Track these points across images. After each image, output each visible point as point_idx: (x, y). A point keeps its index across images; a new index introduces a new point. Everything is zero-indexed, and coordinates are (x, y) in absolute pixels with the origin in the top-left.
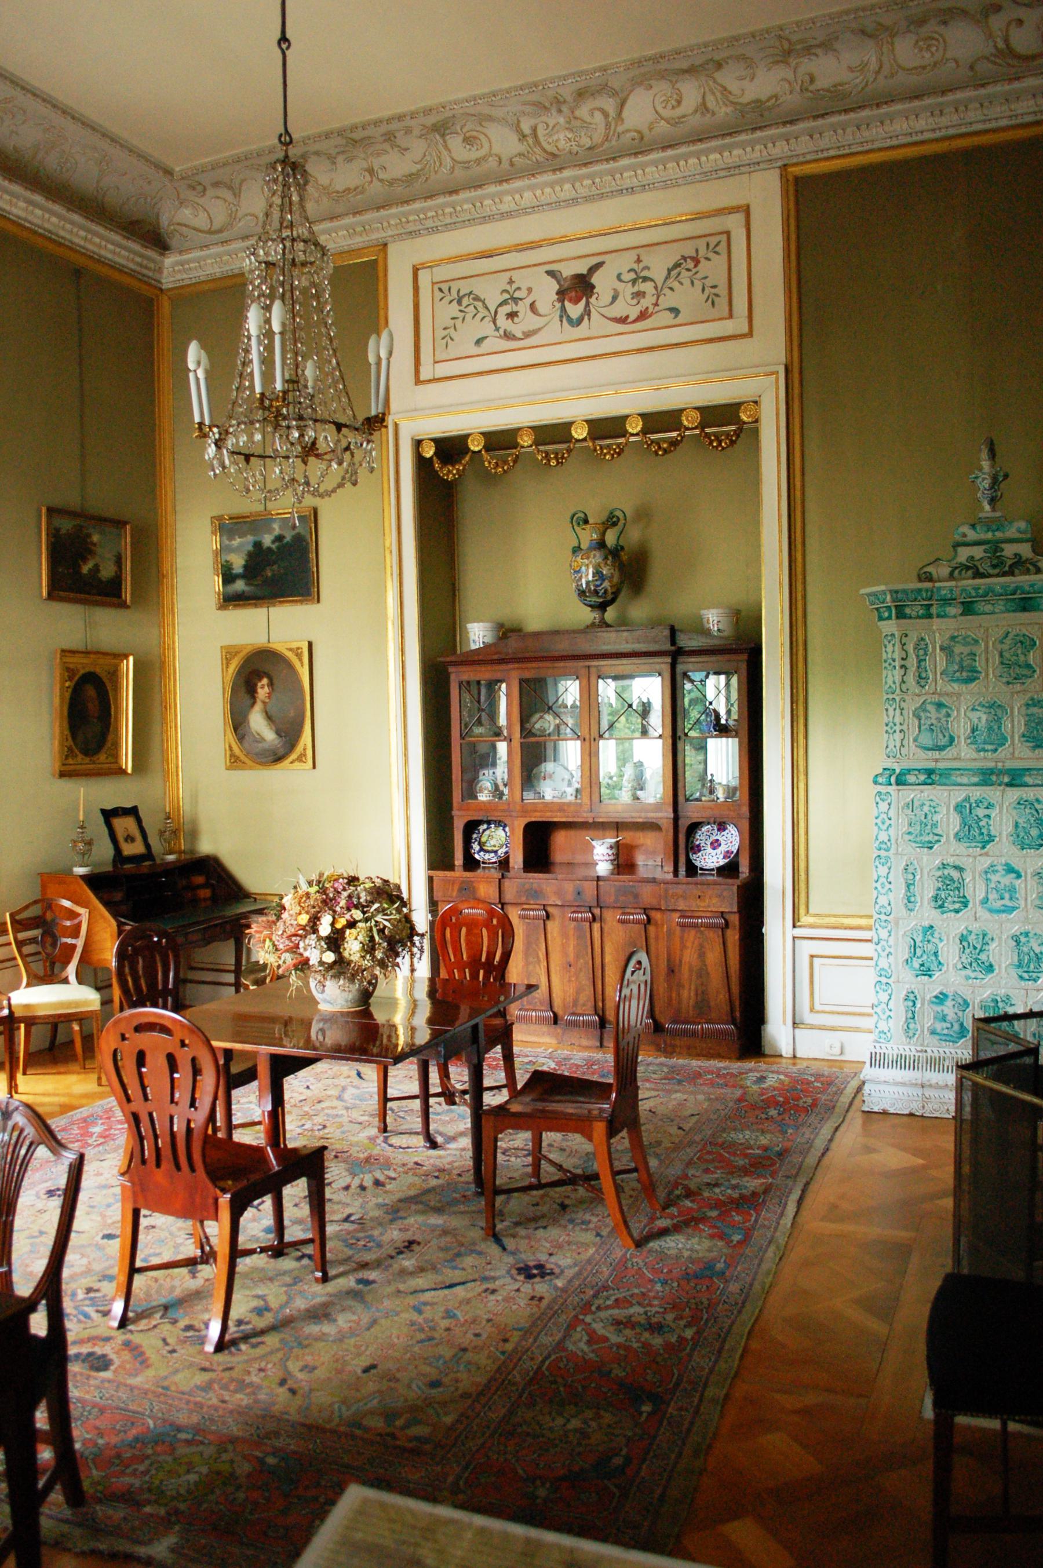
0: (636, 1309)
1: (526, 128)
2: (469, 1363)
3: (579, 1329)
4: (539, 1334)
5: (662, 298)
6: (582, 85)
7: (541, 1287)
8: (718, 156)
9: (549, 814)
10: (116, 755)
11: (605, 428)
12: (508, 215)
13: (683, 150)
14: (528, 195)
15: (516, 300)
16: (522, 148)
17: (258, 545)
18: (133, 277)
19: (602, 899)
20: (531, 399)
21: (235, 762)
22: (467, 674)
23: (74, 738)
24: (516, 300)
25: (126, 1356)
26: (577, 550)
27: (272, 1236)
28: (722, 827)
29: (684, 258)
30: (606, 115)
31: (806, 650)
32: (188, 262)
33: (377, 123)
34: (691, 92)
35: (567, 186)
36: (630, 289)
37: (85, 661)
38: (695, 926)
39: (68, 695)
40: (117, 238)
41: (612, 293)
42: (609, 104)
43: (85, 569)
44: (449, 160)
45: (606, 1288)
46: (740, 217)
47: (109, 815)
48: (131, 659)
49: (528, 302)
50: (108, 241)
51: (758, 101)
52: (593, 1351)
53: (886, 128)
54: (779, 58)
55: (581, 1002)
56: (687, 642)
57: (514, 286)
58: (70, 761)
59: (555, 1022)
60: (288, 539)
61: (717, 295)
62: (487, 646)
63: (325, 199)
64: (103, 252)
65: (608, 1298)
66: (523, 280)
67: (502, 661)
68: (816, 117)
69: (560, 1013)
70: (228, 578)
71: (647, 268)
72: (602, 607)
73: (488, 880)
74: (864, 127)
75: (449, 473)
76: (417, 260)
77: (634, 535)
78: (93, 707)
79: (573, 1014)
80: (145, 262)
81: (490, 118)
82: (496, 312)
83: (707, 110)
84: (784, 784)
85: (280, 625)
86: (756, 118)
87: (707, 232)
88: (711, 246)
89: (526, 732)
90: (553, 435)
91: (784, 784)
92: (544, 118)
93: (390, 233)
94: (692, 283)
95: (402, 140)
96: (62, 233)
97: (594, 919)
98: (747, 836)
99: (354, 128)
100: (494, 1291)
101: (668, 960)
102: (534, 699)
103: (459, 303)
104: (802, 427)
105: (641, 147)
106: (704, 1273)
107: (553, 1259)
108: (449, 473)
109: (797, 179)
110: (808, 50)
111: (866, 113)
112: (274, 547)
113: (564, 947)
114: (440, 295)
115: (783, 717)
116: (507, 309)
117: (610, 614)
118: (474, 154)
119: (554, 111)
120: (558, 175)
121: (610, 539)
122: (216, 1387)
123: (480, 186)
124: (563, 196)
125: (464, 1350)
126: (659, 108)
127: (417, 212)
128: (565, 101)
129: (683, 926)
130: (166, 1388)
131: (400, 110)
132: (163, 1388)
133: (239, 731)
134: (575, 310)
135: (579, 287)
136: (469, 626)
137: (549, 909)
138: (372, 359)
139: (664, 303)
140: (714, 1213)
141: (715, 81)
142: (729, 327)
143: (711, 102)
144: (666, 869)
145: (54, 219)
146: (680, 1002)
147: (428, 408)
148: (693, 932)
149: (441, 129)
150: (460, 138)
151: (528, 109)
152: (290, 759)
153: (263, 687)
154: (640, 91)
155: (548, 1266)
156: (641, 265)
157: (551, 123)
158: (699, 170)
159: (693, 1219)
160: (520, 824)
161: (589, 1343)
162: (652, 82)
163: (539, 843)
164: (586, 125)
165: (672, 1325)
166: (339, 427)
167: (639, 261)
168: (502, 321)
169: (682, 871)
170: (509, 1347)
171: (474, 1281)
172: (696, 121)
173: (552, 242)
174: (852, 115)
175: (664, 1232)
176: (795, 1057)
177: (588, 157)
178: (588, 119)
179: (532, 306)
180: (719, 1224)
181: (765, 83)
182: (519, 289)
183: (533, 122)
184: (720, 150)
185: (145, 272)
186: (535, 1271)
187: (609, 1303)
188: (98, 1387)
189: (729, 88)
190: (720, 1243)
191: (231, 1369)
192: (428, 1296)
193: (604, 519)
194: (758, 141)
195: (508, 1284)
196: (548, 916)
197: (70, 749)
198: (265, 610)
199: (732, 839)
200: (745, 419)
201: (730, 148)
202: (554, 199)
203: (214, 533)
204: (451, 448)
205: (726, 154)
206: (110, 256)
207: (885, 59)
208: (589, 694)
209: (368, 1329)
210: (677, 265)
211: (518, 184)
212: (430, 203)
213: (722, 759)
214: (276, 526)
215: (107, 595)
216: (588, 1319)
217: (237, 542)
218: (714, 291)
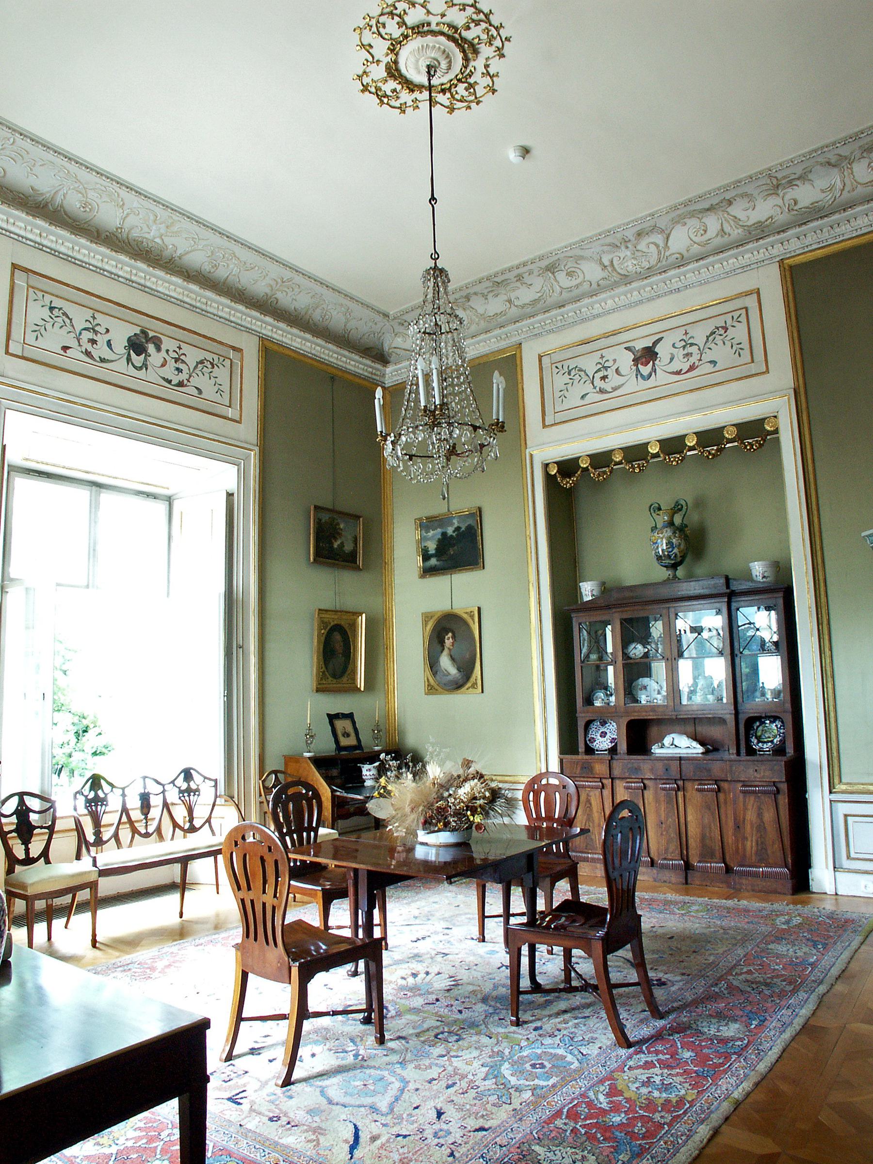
6: (638, 228)
10: (353, 679)
11: (673, 446)
12: (598, 316)
13: (711, 259)
15: (606, 368)
16: (605, 274)
17: (444, 534)
19: (683, 774)
20: (619, 429)
21: (431, 690)
24: (606, 368)
26: (654, 529)
29: (717, 328)
30: (657, 246)
31: (826, 586)
34: (713, 223)
36: (682, 352)
38: (754, 792)
39: (323, 639)
40: (357, 357)
41: (670, 356)
42: (659, 239)
43: (335, 546)
48: (364, 615)
51: (759, 222)
53: (852, 224)
54: (772, 192)
55: (671, 850)
56: (736, 586)
57: (604, 359)
59: (652, 865)
61: (741, 349)
63: (482, 322)
64: (349, 367)
66: (609, 354)
67: (608, 607)
68: (800, 225)
69: (656, 858)
70: (426, 557)
72: (674, 567)
73: (601, 761)
75: (567, 483)
76: (540, 351)
77: (694, 518)
78: (339, 647)
79: (665, 859)
81: (582, 258)
85: (458, 591)
86: (759, 232)
88: (735, 318)
90: (636, 453)
92: (616, 254)
93: (523, 336)
95: (527, 279)
97: (679, 789)
103: (569, 374)
104: (810, 429)
105: (682, 262)
108: (567, 483)
109: (791, 267)
110: (791, 183)
111: (836, 217)
114: (555, 371)
116: (601, 374)
117: (680, 572)
118: (574, 282)
119: (623, 248)
120: (629, 287)
121: (678, 520)
126: (692, 237)
129: (744, 792)
131: (525, 259)
134: (645, 370)
135: (648, 355)
137: (646, 782)
139: (707, 357)
142: (754, 369)
144: (731, 751)
145: (318, 348)
146: (745, 850)
148: (752, 798)
149: (551, 269)
152: (467, 686)
153: (448, 639)
154: (679, 226)
156: (689, 336)
158: (722, 271)
160: (624, 722)
163: (640, 735)
167: (686, 333)
168: (598, 383)
169: (743, 751)
172: (718, 241)
174: (826, 220)
176: (836, 894)
177: (649, 272)
181: (765, 209)
183: (610, 257)
185: (374, 377)
189: (738, 217)
194: (761, 247)
196: (645, 787)
197: (323, 672)
200: (769, 428)
204: (568, 467)
207: (847, 180)
208: (669, 627)
210: (713, 333)
211: (603, 296)
212: (547, 315)
213: (771, 672)
214: (455, 521)
215: (347, 561)
218: (740, 346)
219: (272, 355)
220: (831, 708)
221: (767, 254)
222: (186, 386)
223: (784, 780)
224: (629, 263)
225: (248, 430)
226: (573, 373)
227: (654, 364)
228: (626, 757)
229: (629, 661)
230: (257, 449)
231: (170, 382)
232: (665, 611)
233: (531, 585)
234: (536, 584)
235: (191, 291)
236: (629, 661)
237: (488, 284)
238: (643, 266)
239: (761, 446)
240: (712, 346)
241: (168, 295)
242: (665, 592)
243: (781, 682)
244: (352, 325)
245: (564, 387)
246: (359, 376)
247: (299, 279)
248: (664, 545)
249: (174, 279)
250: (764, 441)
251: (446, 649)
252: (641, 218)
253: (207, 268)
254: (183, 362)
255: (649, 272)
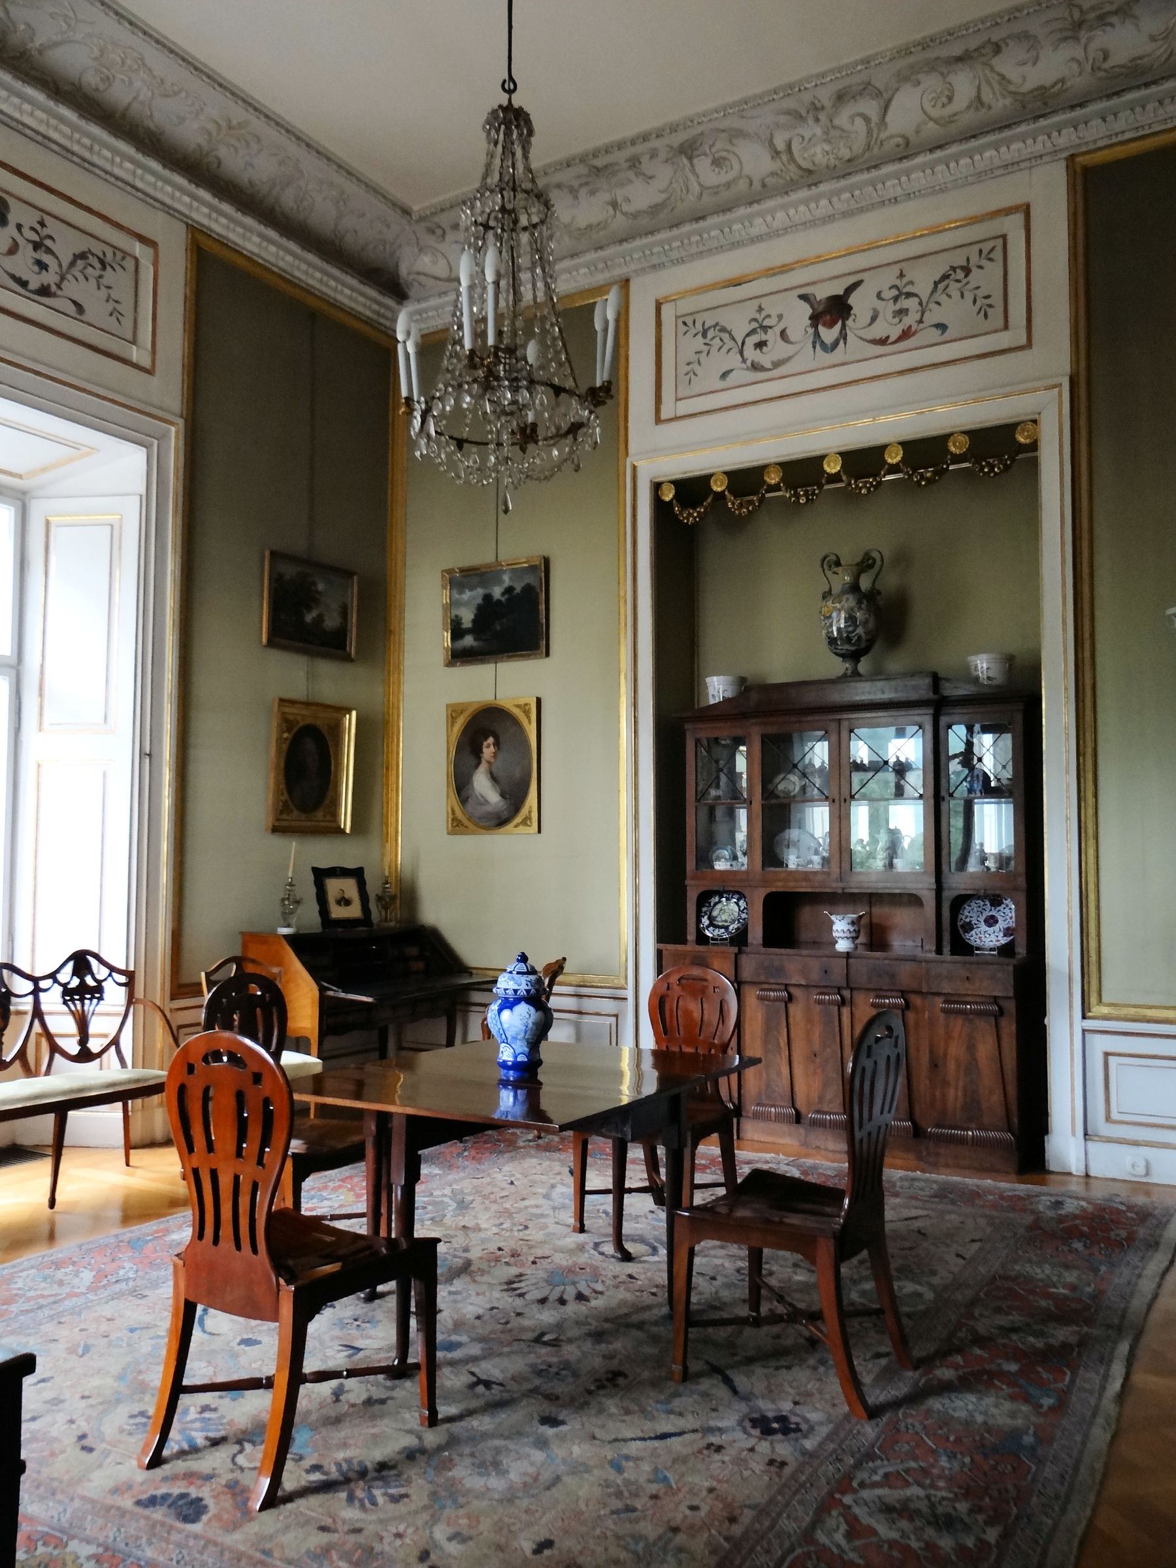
0: (915, 1491)
1: (780, 145)
2: (681, 1550)
3: (834, 1513)
4: (780, 1514)
5: (927, 314)
6: (839, 85)
7: (783, 1449)
8: (994, 153)
9: (792, 884)
10: (334, 813)
11: (863, 462)
12: (759, 239)
13: (954, 149)
14: (780, 215)
15: (765, 329)
16: (775, 166)
17: (487, 598)
18: (371, 326)
21: (457, 826)
22: (705, 732)
23: (290, 792)
24: (765, 329)
25: (227, 1502)
26: (827, 595)
27: (393, 1354)
28: (996, 901)
29: (954, 269)
30: (867, 120)
32: (426, 311)
33: (620, 145)
34: (964, 83)
35: (824, 202)
36: (891, 307)
37: (305, 712)
38: (962, 1012)
39: (285, 747)
40: (354, 282)
41: (870, 314)
42: (870, 107)
44: (695, 184)
45: (870, 1456)
46: (1019, 218)
47: (321, 875)
48: (354, 713)
49: (778, 330)
50: (344, 284)
51: (1042, 87)
52: (854, 1550)
54: (1069, 34)
55: (829, 1096)
57: (764, 314)
58: (285, 817)
60: (518, 589)
61: (990, 306)
62: (726, 700)
63: (566, 238)
64: (340, 298)
65: (875, 1472)
66: (772, 307)
68: (1109, 97)
69: (803, 1110)
70: (457, 632)
71: (912, 283)
72: (854, 657)
74: (1167, 101)
75: (690, 516)
76: (660, 293)
77: (890, 581)
79: (818, 1112)
80: (382, 311)
81: (739, 134)
82: (743, 343)
83: (982, 104)
84: (1069, 850)
85: (507, 682)
86: (1040, 105)
87: (981, 238)
88: (985, 253)
89: (768, 793)
90: (803, 472)
91: (1069, 850)
92: (801, 131)
93: (633, 267)
94: (962, 296)
95: (647, 166)
96: (297, 274)
97: (843, 1002)
98: (1023, 910)
99: (596, 154)
100: (719, 1449)
101: (931, 1052)
102: (777, 757)
103: (704, 335)
105: (906, 151)
106: (1001, 1448)
107: (798, 1409)
108: (690, 516)
110: (1103, 20)
112: (503, 599)
113: (808, 1033)
114: (683, 329)
115: (1067, 772)
116: (755, 339)
117: (864, 666)
118: (724, 178)
119: (811, 121)
121: (865, 583)
122: (335, 1556)
123: (729, 210)
124: (819, 213)
125: (675, 1530)
127: (661, 243)
128: (823, 108)
130: (267, 1553)
131: (645, 127)
132: (264, 1552)
133: (464, 794)
134: (829, 335)
136: (708, 680)
137: (792, 990)
138: (598, 326)
139: (932, 317)
140: (1013, 1367)
141: (992, 70)
142: (1004, 340)
143: (987, 96)
144: (927, 947)
145: (289, 258)
147: (670, 446)
148: (959, 1021)
149: (688, 150)
150: (709, 160)
151: (783, 119)
153: (488, 747)
155: (794, 1419)
157: (807, 136)
159: (985, 1372)
160: (758, 897)
161: (850, 1536)
162: (921, 77)
164: (844, 134)
165: (967, 1519)
166: (558, 390)
167: (902, 275)
168: (751, 353)
170: (737, 1530)
171: (694, 1431)
172: (969, 119)
173: (803, 263)
174: (1154, 89)
175: (945, 1388)
176: (1087, 1176)
177: (848, 168)
178: (846, 125)
179: (783, 334)
180: (1022, 1382)
182: (769, 316)
183: (786, 135)
184: (996, 146)
185: (382, 321)
186: (775, 1425)
187: (876, 1478)
188: (179, 1545)
190: (1025, 1408)
191: (359, 1531)
192: (634, 1448)
193: (858, 559)
195: (739, 1440)
197: (285, 804)
198: (492, 666)
199: (1009, 914)
200: (1022, 440)
201: (1008, 142)
202: (809, 217)
203: (444, 587)
204: (692, 489)
205: (1003, 149)
206: (346, 301)
208: (839, 752)
209: (548, 1488)
210: (945, 277)
211: (769, 204)
212: (675, 232)
213: (994, 828)
216: (847, 1500)
217: (467, 595)
218: (988, 301)
219: (209, 263)
220: (1091, 887)
221: (1048, 145)
222: (54, 295)
223: (1011, 994)
224: (818, 149)
225: (168, 388)
226: (710, 334)
227: (844, 326)
228: (763, 950)
229: (773, 801)
230: (181, 422)
231: (24, 284)
232: (833, 726)
233: (622, 677)
234: (630, 675)
235: (62, 119)
236: (773, 801)
237: (582, 169)
238: (840, 154)
239: (1007, 468)
240: (943, 298)
241: (17, 121)
242: (838, 696)
243: (1012, 843)
244: (348, 223)
245: (694, 358)
246: (357, 316)
247: (258, 124)
248: (842, 621)
249: (30, 91)
250: (1013, 460)
251: (483, 761)
252: (847, 66)
253: (91, 80)
254: (49, 251)
255: (848, 168)
